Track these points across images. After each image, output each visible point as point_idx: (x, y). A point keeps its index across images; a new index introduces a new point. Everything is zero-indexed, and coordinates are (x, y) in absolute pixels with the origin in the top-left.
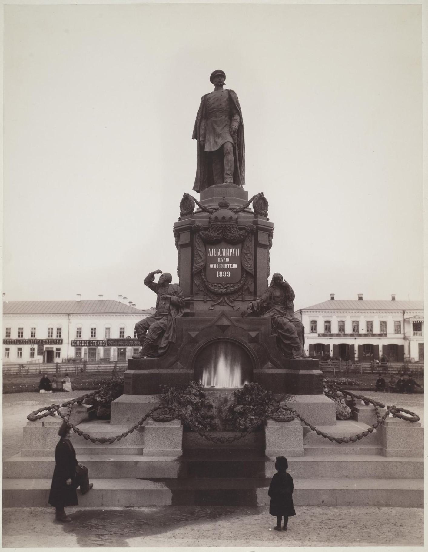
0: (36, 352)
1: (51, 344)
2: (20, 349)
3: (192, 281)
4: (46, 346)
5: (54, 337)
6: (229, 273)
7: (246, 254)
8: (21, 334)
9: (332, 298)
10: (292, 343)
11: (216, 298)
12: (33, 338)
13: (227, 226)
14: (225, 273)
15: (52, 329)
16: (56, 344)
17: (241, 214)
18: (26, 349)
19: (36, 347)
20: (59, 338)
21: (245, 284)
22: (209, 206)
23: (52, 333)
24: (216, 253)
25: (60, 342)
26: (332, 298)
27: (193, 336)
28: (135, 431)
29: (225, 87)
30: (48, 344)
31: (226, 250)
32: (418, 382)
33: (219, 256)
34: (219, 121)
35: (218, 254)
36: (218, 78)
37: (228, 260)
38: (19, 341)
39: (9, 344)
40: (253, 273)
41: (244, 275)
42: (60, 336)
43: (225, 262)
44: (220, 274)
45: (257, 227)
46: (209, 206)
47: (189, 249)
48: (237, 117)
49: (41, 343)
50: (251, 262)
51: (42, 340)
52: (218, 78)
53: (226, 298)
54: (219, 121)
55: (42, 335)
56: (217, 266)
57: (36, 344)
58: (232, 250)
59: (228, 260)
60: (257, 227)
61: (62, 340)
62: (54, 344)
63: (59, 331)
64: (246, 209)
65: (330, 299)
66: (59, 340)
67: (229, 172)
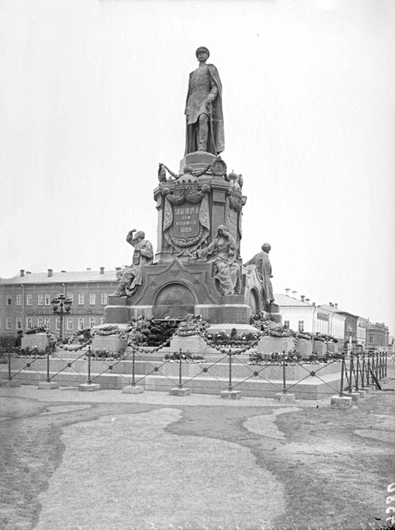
3: (163, 237)
10: (225, 283)
13: (187, 188)
14: (187, 229)
17: (204, 177)
21: (202, 237)
28: (23, 346)
29: (208, 62)
36: (202, 53)
41: (202, 230)
45: (211, 188)
47: (161, 211)
48: (214, 90)
50: (207, 218)
52: (202, 53)
63: (301, 324)
64: (207, 172)
67: (201, 141)
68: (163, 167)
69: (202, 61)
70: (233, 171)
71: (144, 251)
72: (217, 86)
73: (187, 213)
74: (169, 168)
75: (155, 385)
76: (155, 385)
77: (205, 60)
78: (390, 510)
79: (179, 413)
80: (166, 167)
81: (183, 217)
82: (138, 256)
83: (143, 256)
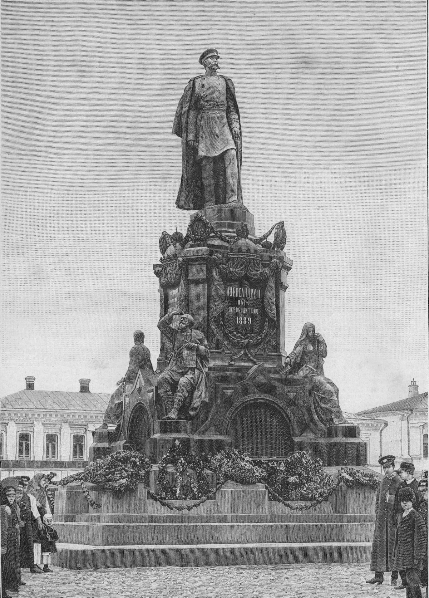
9: (30, 386)
11: (236, 351)
22: (226, 232)
26: (30, 386)
32: (242, 521)
33: (238, 298)
34: (205, 111)
36: (208, 57)
37: (248, 303)
40: (275, 319)
43: (246, 306)
44: (240, 321)
46: (226, 232)
52: (208, 57)
54: (205, 111)
56: (236, 310)
59: (248, 303)
65: (24, 386)
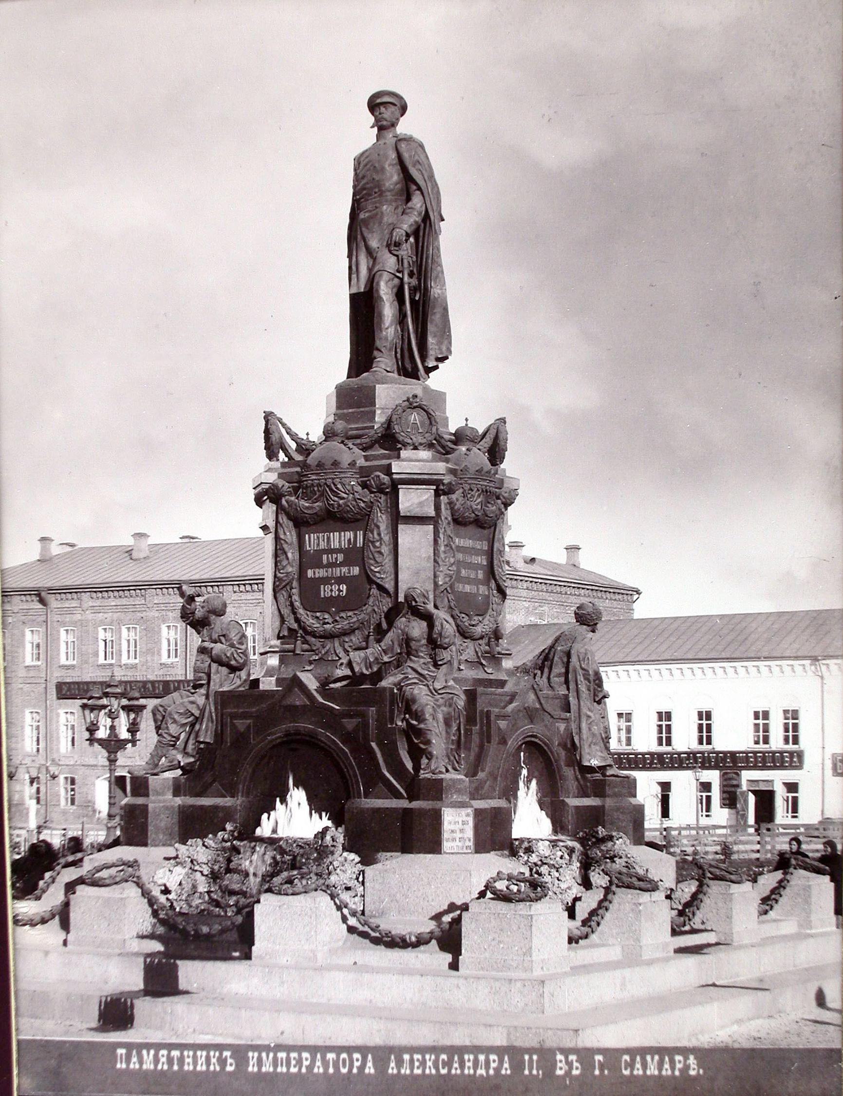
0: (716, 794)
1: (764, 768)
2: (666, 787)
4: (747, 776)
5: (777, 742)
6: (344, 587)
7: (373, 542)
8: (665, 734)
12: (705, 747)
14: (335, 587)
15: (766, 715)
16: (782, 767)
18: (684, 782)
19: (713, 776)
20: (791, 747)
23: (766, 729)
24: (318, 545)
25: (794, 760)
27: (242, 728)
30: (755, 767)
31: (336, 534)
35: (323, 545)
36: (384, 107)
37: (340, 557)
38: (660, 756)
39: (673, 768)
42: (796, 741)
48: (417, 201)
49: (730, 763)
51: (733, 754)
53: (337, 644)
55: (733, 736)
56: (321, 573)
57: (716, 767)
58: (349, 535)
60: (392, 480)
61: (800, 755)
62: (775, 768)
66: (791, 754)
68: (272, 420)
69: (383, 127)
70: (467, 420)
71: (218, 648)
72: (422, 194)
73: (335, 544)
74: (289, 425)
75: (551, 841)
76: (551, 841)
77: (393, 125)
78: (31, 799)
79: (284, 806)
80: (280, 420)
81: (325, 557)
82: (207, 664)
83: (221, 663)
